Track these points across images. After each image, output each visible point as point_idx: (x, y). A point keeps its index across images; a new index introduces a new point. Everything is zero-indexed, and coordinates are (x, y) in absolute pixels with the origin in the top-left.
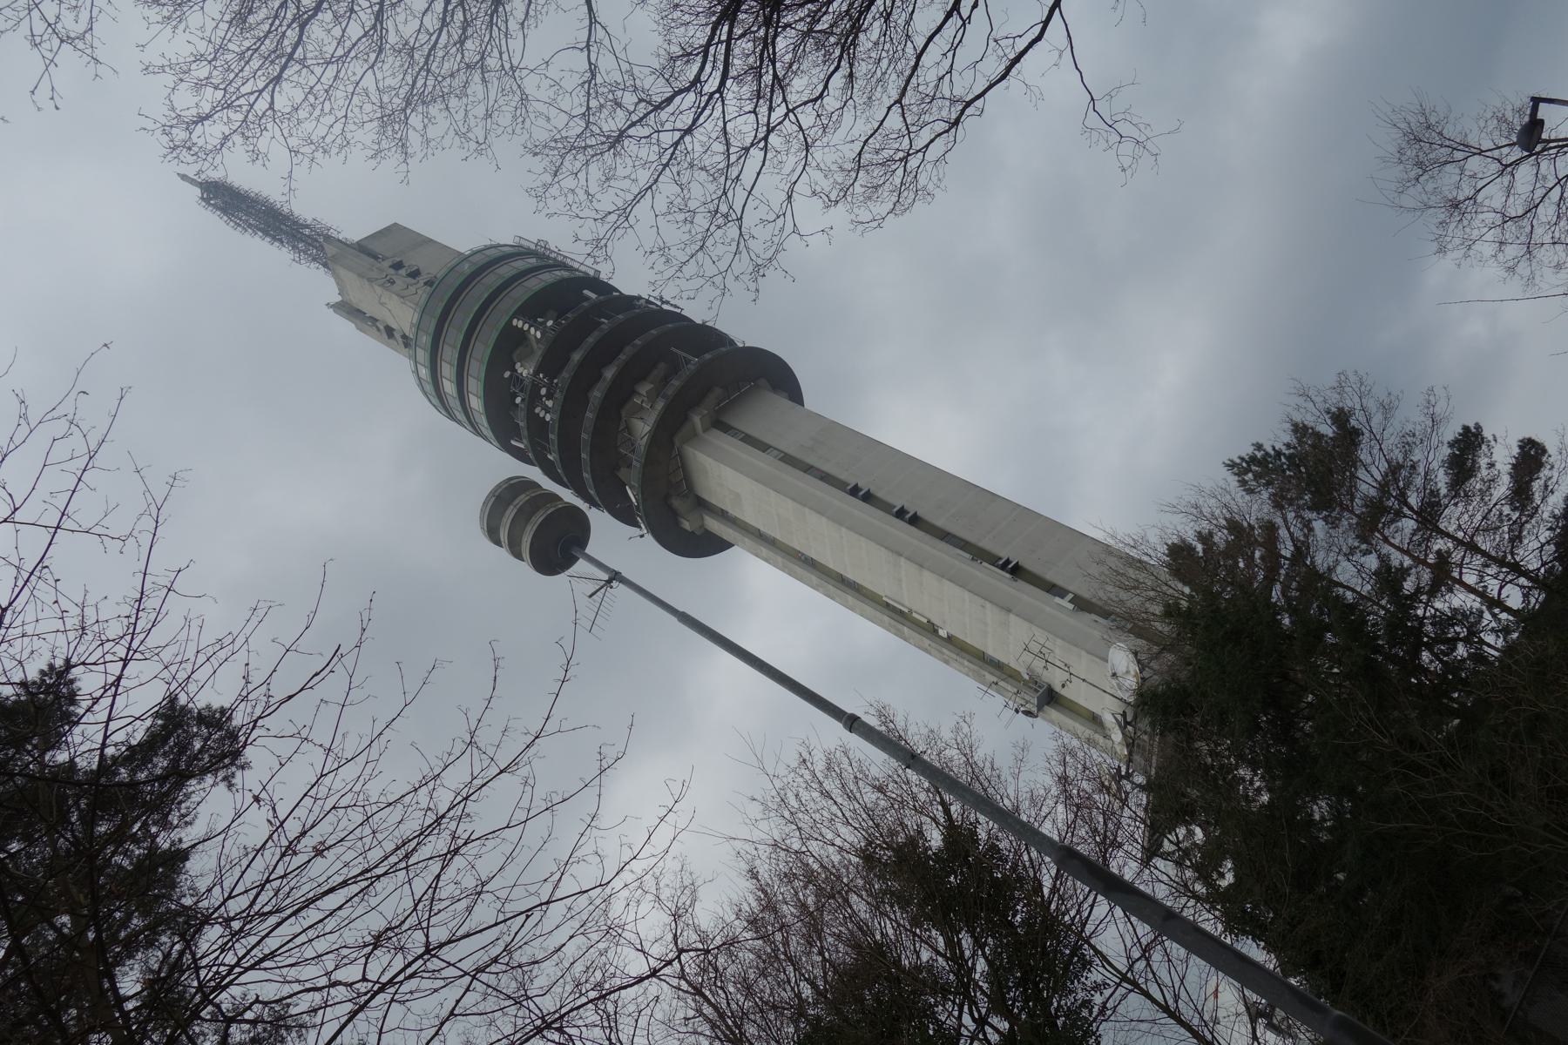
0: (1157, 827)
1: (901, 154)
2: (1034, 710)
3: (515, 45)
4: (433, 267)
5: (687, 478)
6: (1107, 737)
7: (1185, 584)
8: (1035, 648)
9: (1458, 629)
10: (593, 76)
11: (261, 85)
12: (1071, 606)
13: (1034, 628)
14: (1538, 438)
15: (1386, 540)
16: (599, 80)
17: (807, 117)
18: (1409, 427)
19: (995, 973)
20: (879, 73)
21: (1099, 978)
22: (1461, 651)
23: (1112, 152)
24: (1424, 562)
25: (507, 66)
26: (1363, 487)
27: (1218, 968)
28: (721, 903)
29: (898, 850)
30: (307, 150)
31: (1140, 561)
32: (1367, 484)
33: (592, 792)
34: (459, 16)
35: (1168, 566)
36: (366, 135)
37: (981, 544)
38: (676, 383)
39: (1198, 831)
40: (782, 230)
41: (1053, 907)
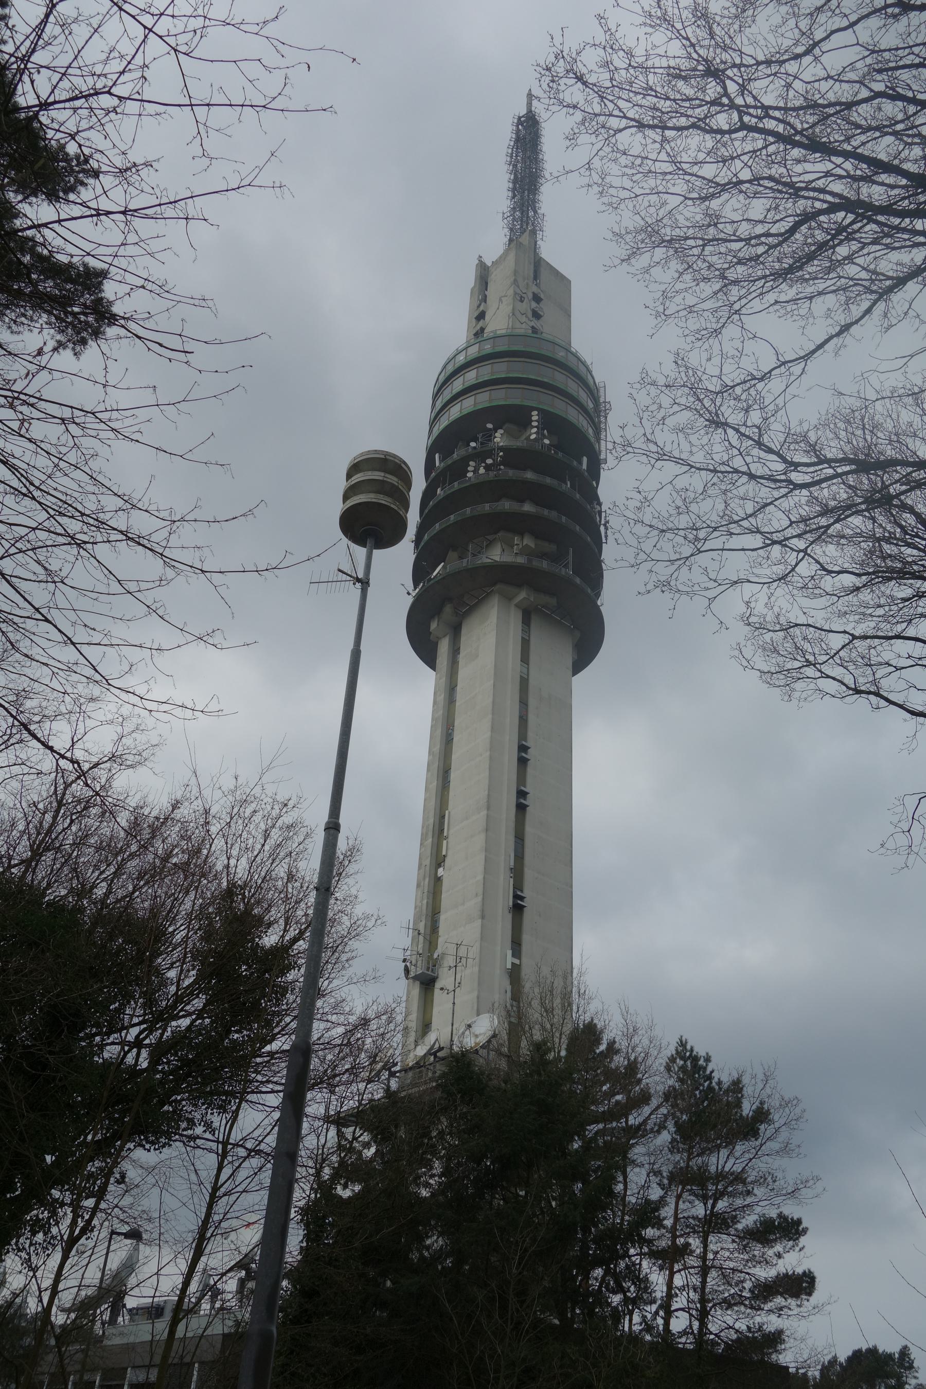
0: (361, 1117)
1: (811, 658)
2: (412, 974)
3: (756, 305)
4: (548, 327)
5: (472, 609)
6: (416, 1044)
7: (567, 1050)
8: (462, 952)
9: (632, 1289)
10: (761, 379)
11: (630, 114)
12: (509, 966)
13: (478, 944)
14: (819, 1284)
15: (679, 1197)
16: (760, 386)
17: (806, 569)
18: (779, 1175)
19: (180, 1039)
20: (870, 611)
21: (216, 1124)
22: (616, 1299)
23: (892, 829)
24: (674, 1237)
25: (737, 307)
26: (713, 1159)
27: (267, 1217)
28: (143, 788)
29: (248, 912)
30: (596, 178)
31: (570, 1005)
32: (718, 1161)
33: (179, 638)
34: (761, 250)
35: (576, 1029)
36: (630, 221)
37: (526, 870)
38: (545, 565)
39: (373, 1150)
40: (707, 589)
41: (259, 1060)
